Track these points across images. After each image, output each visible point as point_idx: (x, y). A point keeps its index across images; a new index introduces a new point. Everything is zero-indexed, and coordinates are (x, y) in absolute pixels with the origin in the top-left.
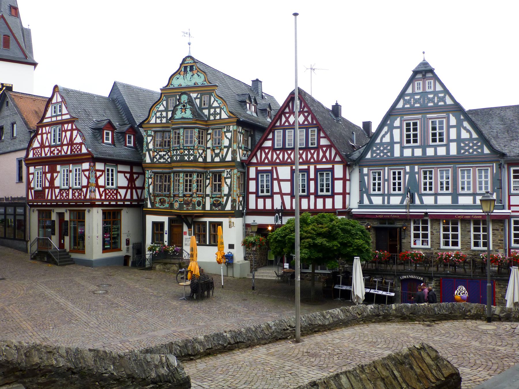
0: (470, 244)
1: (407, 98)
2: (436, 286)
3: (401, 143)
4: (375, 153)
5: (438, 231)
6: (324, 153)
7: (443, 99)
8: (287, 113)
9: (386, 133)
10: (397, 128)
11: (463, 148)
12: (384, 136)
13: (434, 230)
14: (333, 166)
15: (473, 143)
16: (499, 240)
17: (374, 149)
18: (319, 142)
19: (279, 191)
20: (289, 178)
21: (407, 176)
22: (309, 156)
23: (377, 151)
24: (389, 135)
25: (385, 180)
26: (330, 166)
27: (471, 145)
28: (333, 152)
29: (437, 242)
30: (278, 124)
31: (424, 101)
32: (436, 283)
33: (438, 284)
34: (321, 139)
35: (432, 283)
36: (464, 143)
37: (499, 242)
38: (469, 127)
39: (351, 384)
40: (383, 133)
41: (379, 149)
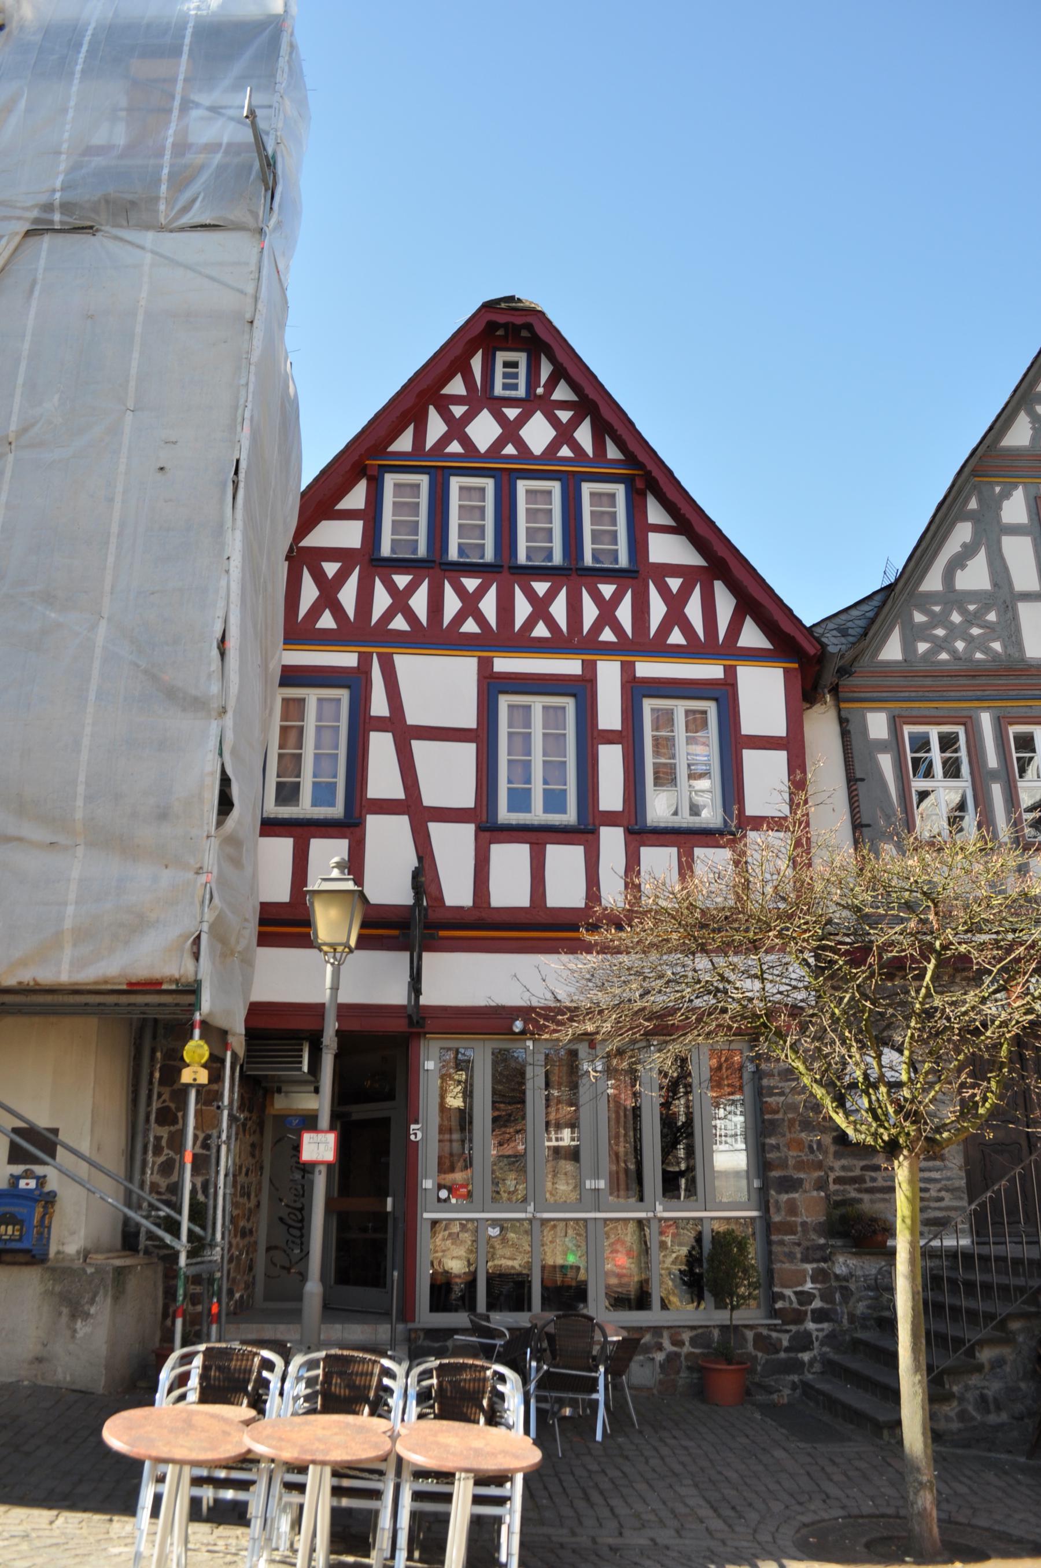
4: (925, 640)
6: (676, 604)
8: (457, 400)
9: (968, 552)
12: (958, 562)
14: (731, 672)
17: (919, 618)
18: (638, 546)
19: (399, 794)
20: (469, 720)
22: (590, 612)
23: (935, 627)
26: (713, 671)
28: (725, 605)
30: (404, 443)
34: (653, 538)
39: (233, 288)
40: (952, 546)
41: (941, 620)
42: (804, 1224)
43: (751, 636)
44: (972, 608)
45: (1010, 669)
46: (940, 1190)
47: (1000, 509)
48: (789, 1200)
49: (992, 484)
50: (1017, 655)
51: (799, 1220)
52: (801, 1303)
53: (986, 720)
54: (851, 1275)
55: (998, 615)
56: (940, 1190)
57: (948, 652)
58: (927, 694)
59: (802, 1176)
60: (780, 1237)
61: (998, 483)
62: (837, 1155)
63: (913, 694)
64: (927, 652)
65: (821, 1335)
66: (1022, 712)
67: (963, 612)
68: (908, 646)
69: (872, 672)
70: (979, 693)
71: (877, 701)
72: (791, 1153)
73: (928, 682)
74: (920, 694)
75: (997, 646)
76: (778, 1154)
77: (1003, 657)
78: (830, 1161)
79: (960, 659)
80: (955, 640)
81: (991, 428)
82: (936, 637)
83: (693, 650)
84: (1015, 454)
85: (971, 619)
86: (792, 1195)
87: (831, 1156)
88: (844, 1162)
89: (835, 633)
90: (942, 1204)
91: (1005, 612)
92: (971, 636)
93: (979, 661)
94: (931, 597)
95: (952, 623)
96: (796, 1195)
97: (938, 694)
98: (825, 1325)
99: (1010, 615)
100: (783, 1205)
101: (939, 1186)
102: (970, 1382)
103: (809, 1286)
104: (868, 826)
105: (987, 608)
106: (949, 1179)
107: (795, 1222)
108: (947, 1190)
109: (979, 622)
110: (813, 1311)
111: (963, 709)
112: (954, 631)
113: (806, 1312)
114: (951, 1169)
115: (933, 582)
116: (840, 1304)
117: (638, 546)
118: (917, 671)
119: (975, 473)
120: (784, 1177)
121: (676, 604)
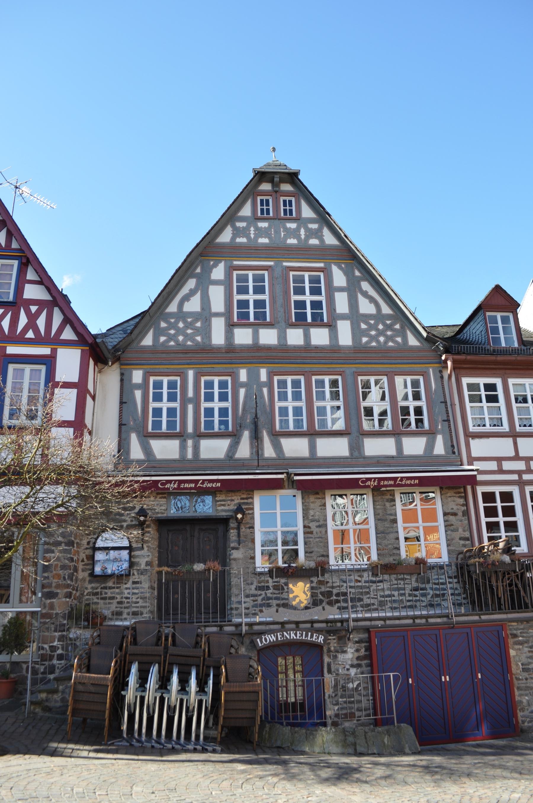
0: (398, 552)
1: (241, 225)
2: (358, 658)
3: (228, 314)
4: (164, 336)
5: (321, 523)
6: (32, 318)
7: (318, 234)
9: (192, 293)
10: (217, 283)
11: (365, 333)
12: (187, 298)
13: (313, 521)
14: (54, 352)
15: (384, 324)
16: (461, 539)
17: (163, 325)
18: (19, 290)
21: (242, 392)
23: (170, 329)
24: (198, 296)
25: (185, 401)
26: (46, 351)
27: (381, 327)
28: (57, 318)
29: (321, 551)
31: (277, 232)
32: (357, 650)
33: (363, 652)
34: (28, 287)
35: (345, 652)
36: (366, 323)
37: (462, 542)
38: (372, 292)
40: (185, 290)
41: (174, 326)
42: (57, 614)
43: (68, 334)
44: (189, 320)
45: (203, 350)
46: (137, 598)
47: (211, 272)
48: (50, 602)
49: (209, 260)
50: (208, 343)
51: (55, 612)
52: (52, 651)
53: (191, 374)
54: (77, 638)
55: (202, 324)
56: (137, 598)
57: (175, 342)
58: (163, 361)
59: (59, 591)
60: (44, 620)
61: (212, 260)
62: (90, 582)
63: (156, 362)
64: (165, 341)
65: (60, 666)
66: (209, 370)
67: (185, 322)
68: (156, 338)
69: (137, 351)
70: (188, 361)
71: (137, 365)
72: (54, 580)
73: (164, 355)
74: (160, 361)
75: (199, 338)
76: (48, 581)
77: (201, 344)
78: (87, 585)
79: (180, 345)
80: (179, 336)
81: (208, 234)
82: (170, 334)
83: (38, 341)
84: (223, 246)
85: (188, 326)
86: (52, 600)
87: (87, 582)
88: (93, 585)
89: (121, 332)
90: (137, 605)
91: (205, 322)
92: (187, 334)
93: (189, 345)
94: (171, 315)
95: (179, 327)
96: (54, 600)
97: (168, 362)
98: (63, 662)
99: (207, 323)
100: (47, 605)
101: (137, 596)
102: (68, 685)
103: (55, 644)
104: (125, 425)
105: (197, 320)
106: (142, 593)
107: (52, 613)
108: (141, 598)
109: (191, 327)
110: (58, 655)
111: (180, 368)
112: (179, 331)
113: (54, 656)
114: (144, 588)
115: (172, 308)
116: (71, 651)
117: (19, 290)
118: (158, 351)
119: (201, 255)
120: (50, 592)
121: (32, 318)
